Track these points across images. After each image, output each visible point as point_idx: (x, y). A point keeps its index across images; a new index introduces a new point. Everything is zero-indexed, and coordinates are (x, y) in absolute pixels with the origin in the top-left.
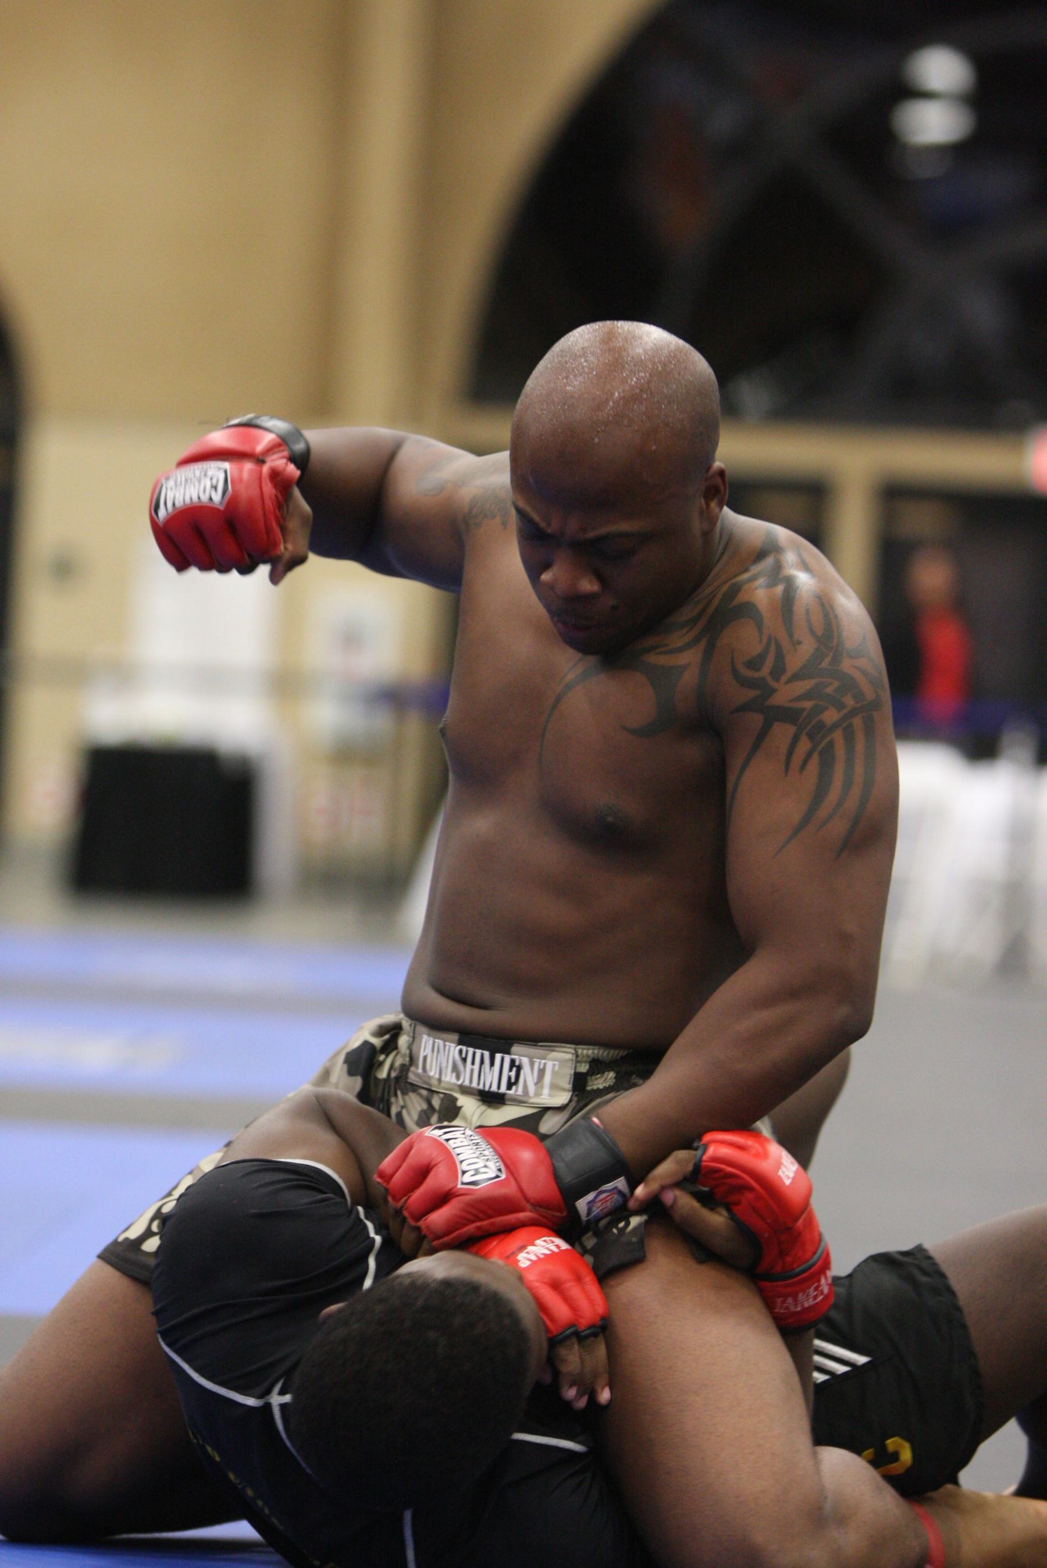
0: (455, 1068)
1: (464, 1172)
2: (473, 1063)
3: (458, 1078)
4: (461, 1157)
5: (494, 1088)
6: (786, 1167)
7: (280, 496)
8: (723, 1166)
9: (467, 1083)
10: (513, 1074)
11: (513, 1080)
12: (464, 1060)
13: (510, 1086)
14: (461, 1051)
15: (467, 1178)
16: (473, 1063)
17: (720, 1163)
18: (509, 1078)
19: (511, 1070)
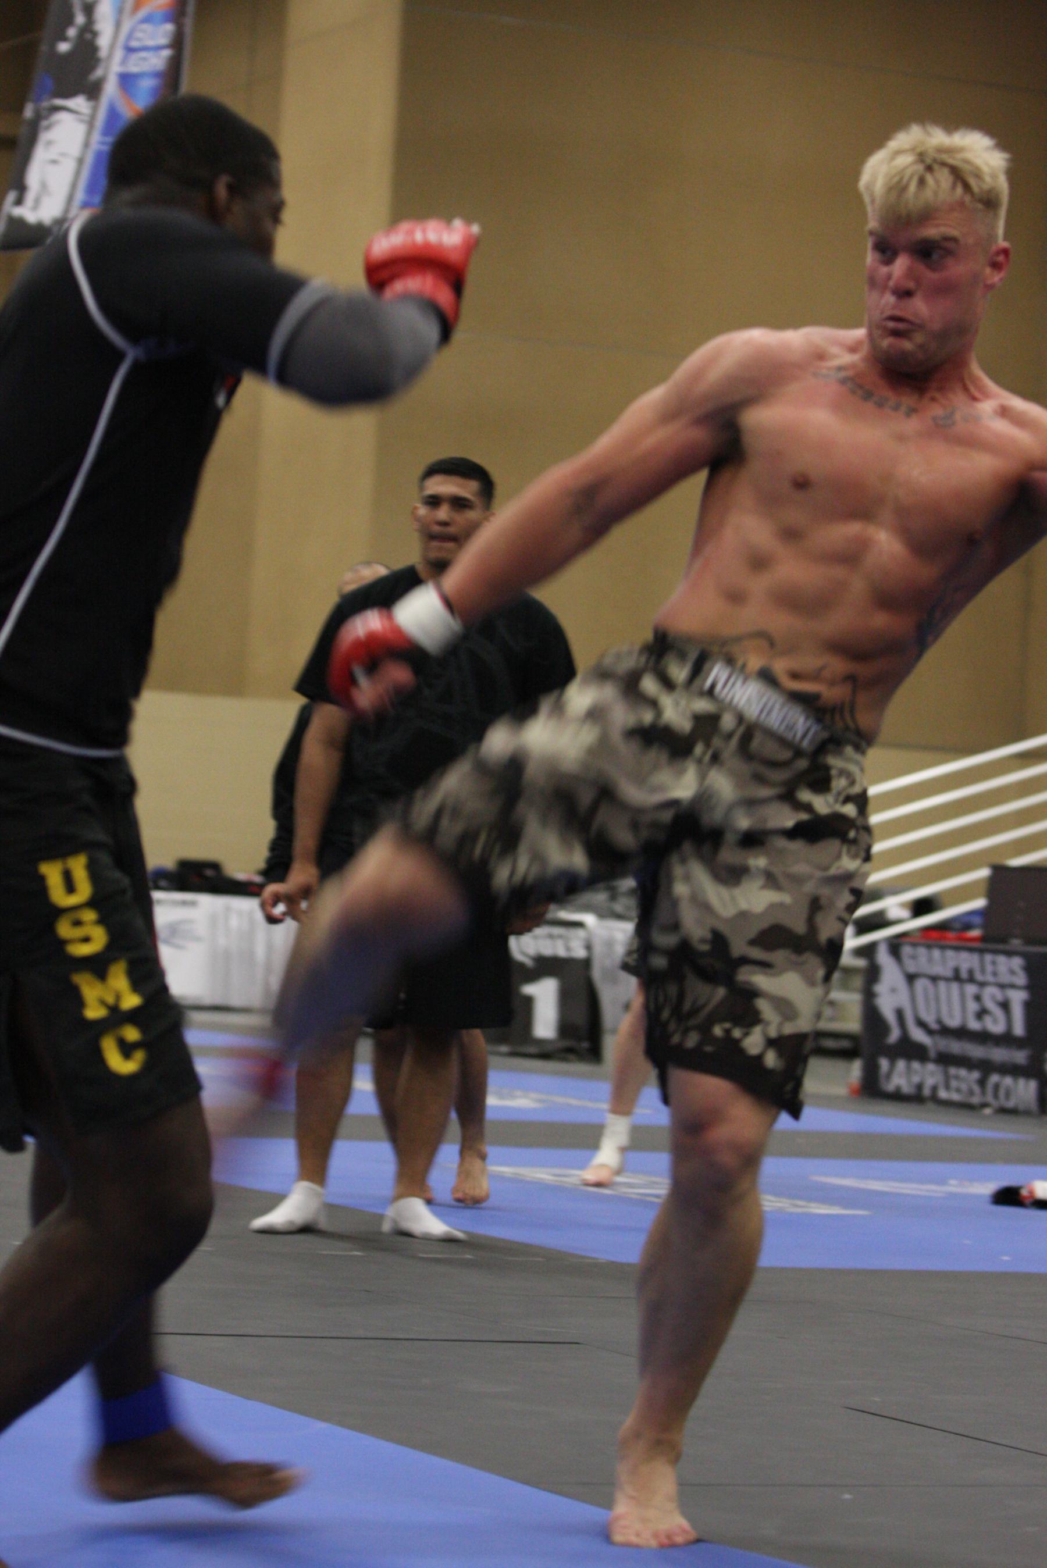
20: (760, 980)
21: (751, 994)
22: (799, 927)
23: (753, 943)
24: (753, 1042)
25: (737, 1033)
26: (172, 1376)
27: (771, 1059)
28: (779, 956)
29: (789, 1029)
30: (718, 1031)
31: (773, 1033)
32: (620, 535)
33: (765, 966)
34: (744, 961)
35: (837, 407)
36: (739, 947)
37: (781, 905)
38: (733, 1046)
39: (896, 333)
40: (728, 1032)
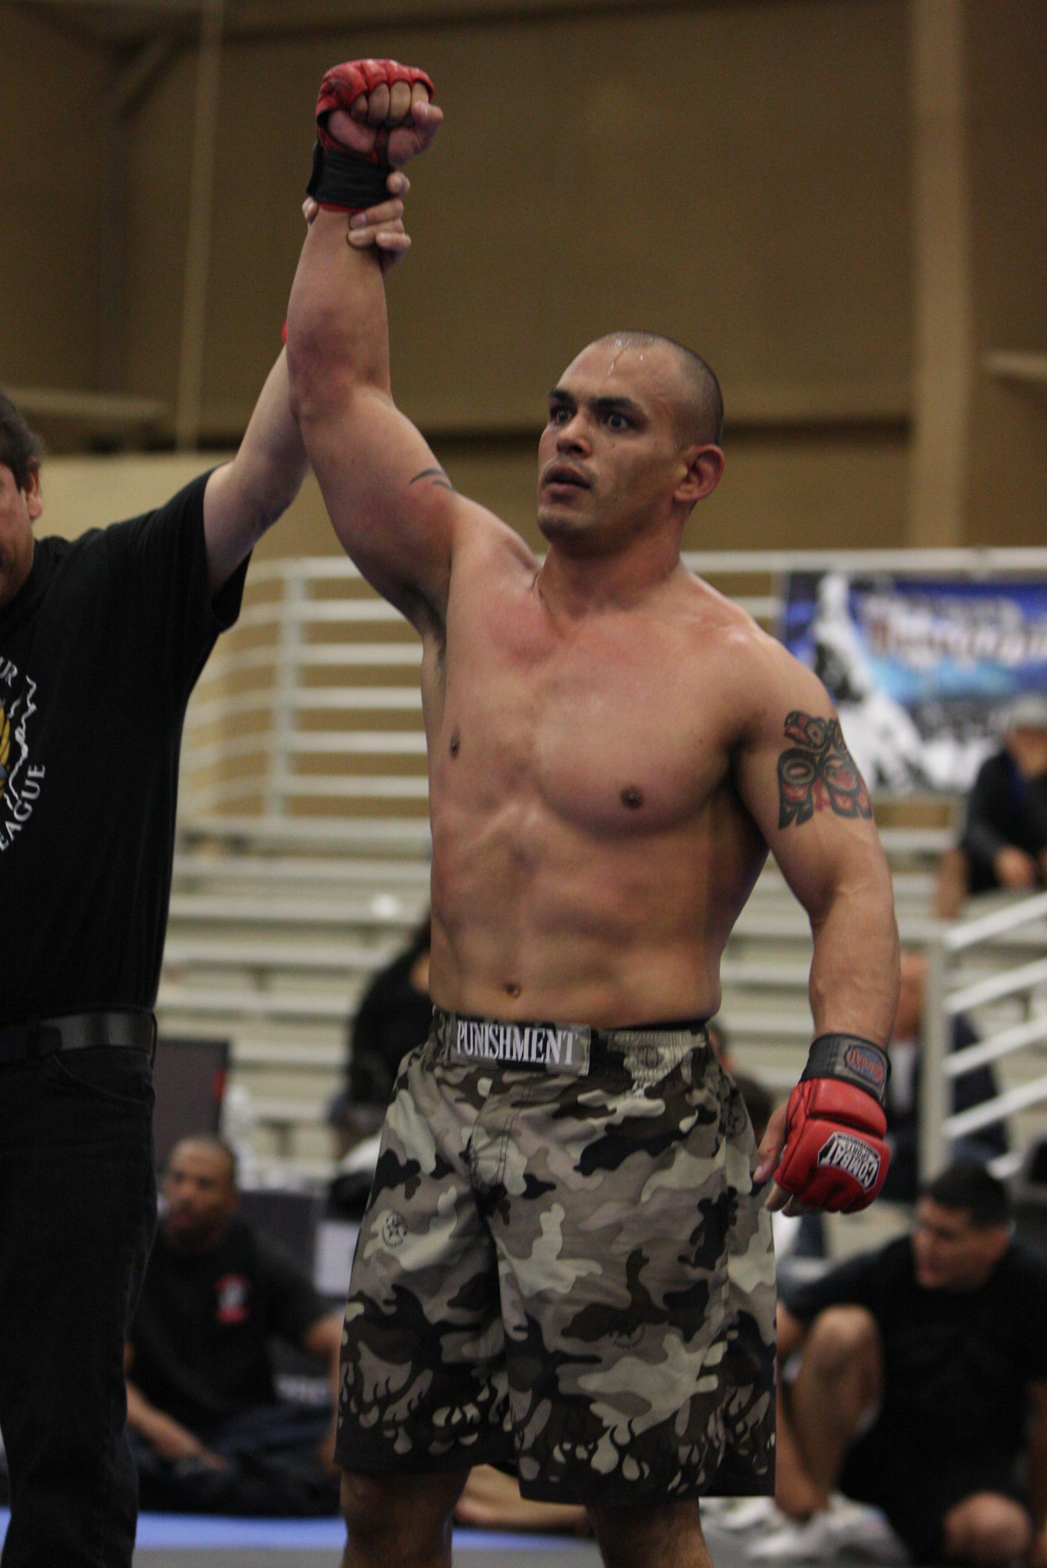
0: (491, 1045)
1: (863, 1181)
2: (505, 1037)
3: (494, 1052)
4: (855, 1172)
5: (526, 1058)
6: (413, 1095)
7: (794, 821)
8: (808, 1108)
9: (501, 1056)
10: (541, 1044)
11: (541, 1049)
12: (498, 1038)
13: (539, 1055)
14: (494, 1031)
15: (867, 1183)
16: (505, 1037)
17: (12, 768)
18: (538, 1049)
19: (538, 1041)
20: (592, 1382)
21: (584, 1401)
22: (619, 1295)
23: (566, 1333)
24: (604, 1459)
25: (581, 1453)
26: (429, 964)
27: (631, 1471)
28: (605, 1347)
29: (640, 1426)
30: (558, 1455)
31: (623, 1438)
32: (155, 1064)
33: (592, 1361)
34: (565, 1358)
35: (482, 1340)
36: (554, 1341)
37: (397, 244)
38: (579, 1469)
39: (557, 499)
40: (570, 1455)
